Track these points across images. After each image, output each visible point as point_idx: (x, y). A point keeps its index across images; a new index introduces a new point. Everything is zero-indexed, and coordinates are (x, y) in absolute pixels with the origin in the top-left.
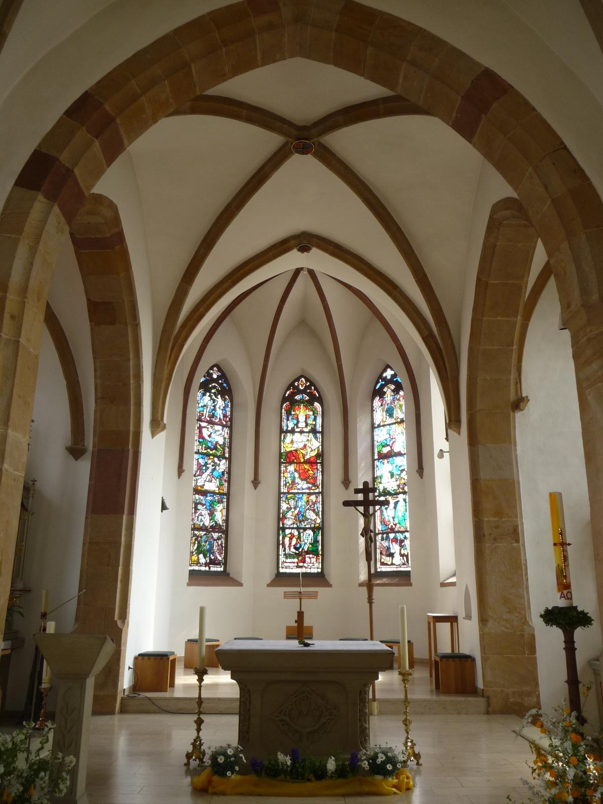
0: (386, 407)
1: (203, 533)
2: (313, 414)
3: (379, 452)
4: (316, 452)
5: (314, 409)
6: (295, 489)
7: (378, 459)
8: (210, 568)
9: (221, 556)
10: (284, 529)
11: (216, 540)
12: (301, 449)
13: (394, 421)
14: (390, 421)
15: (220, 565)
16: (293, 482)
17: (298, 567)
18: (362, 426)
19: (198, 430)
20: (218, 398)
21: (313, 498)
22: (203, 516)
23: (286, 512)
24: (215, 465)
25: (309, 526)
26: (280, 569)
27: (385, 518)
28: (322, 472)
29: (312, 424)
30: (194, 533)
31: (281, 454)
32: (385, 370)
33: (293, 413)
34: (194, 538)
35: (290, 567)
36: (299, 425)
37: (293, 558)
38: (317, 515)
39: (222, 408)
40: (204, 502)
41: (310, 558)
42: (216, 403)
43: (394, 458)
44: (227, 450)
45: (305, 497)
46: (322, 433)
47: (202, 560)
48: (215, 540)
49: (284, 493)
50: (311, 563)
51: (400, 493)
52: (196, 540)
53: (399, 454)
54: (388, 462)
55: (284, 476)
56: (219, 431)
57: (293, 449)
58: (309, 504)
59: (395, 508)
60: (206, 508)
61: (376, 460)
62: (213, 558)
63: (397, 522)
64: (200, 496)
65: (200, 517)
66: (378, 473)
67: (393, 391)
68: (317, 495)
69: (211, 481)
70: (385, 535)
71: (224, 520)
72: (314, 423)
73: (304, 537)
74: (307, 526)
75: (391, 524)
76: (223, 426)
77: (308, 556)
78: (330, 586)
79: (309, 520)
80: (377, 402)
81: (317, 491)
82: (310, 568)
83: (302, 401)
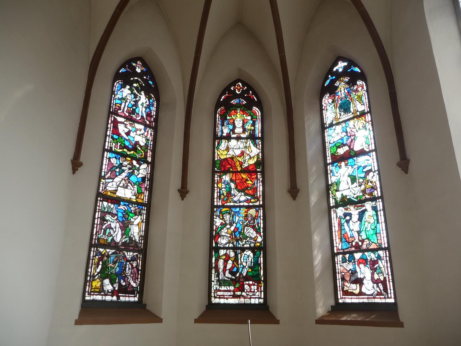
0: (340, 102)
1: (111, 251)
2: (252, 119)
3: (333, 155)
4: (255, 160)
5: (252, 114)
6: (230, 202)
7: (332, 163)
8: (118, 297)
9: (135, 282)
10: (217, 249)
11: (129, 261)
12: (238, 156)
13: (352, 116)
14: (345, 117)
15: (134, 294)
16: (229, 194)
17: (234, 296)
18: (311, 127)
19: (112, 125)
20: (142, 95)
21: (252, 212)
22: (112, 229)
23: (219, 229)
24: (132, 168)
25: (248, 246)
26: (213, 299)
27: (346, 233)
28: (263, 182)
29: (250, 130)
30: (97, 250)
31: (214, 162)
32: (336, 64)
33: (228, 118)
34: (97, 257)
35: (224, 297)
36: (235, 130)
37: (229, 286)
38: (258, 232)
39: (145, 105)
40: (114, 212)
41: (249, 285)
42: (138, 99)
43: (355, 158)
44: (149, 153)
45: (243, 210)
46: (262, 139)
47: (108, 287)
48: (128, 261)
49: (218, 207)
50: (251, 291)
51: (366, 200)
52: (100, 260)
53: (362, 153)
54: (346, 165)
55: (218, 187)
56: (140, 130)
57: (228, 156)
58: (247, 220)
59: (360, 219)
60: (117, 219)
61: (329, 164)
62: (124, 284)
63: (364, 237)
64: (110, 204)
65: (108, 231)
66: (332, 179)
67: (347, 83)
68: (257, 209)
69: (126, 187)
70: (347, 256)
71: (141, 236)
72: (253, 128)
73: (242, 258)
74: (245, 246)
75: (356, 241)
76: (146, 126)
77: (247, 282)
78: (277, 322)
79: (248, 239)
80: (327, 100)
81: (257, 204)
82: (250, 298)
83: (238, 105)
